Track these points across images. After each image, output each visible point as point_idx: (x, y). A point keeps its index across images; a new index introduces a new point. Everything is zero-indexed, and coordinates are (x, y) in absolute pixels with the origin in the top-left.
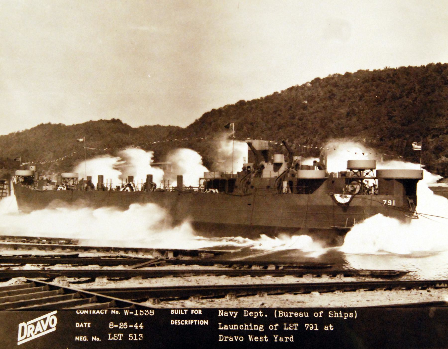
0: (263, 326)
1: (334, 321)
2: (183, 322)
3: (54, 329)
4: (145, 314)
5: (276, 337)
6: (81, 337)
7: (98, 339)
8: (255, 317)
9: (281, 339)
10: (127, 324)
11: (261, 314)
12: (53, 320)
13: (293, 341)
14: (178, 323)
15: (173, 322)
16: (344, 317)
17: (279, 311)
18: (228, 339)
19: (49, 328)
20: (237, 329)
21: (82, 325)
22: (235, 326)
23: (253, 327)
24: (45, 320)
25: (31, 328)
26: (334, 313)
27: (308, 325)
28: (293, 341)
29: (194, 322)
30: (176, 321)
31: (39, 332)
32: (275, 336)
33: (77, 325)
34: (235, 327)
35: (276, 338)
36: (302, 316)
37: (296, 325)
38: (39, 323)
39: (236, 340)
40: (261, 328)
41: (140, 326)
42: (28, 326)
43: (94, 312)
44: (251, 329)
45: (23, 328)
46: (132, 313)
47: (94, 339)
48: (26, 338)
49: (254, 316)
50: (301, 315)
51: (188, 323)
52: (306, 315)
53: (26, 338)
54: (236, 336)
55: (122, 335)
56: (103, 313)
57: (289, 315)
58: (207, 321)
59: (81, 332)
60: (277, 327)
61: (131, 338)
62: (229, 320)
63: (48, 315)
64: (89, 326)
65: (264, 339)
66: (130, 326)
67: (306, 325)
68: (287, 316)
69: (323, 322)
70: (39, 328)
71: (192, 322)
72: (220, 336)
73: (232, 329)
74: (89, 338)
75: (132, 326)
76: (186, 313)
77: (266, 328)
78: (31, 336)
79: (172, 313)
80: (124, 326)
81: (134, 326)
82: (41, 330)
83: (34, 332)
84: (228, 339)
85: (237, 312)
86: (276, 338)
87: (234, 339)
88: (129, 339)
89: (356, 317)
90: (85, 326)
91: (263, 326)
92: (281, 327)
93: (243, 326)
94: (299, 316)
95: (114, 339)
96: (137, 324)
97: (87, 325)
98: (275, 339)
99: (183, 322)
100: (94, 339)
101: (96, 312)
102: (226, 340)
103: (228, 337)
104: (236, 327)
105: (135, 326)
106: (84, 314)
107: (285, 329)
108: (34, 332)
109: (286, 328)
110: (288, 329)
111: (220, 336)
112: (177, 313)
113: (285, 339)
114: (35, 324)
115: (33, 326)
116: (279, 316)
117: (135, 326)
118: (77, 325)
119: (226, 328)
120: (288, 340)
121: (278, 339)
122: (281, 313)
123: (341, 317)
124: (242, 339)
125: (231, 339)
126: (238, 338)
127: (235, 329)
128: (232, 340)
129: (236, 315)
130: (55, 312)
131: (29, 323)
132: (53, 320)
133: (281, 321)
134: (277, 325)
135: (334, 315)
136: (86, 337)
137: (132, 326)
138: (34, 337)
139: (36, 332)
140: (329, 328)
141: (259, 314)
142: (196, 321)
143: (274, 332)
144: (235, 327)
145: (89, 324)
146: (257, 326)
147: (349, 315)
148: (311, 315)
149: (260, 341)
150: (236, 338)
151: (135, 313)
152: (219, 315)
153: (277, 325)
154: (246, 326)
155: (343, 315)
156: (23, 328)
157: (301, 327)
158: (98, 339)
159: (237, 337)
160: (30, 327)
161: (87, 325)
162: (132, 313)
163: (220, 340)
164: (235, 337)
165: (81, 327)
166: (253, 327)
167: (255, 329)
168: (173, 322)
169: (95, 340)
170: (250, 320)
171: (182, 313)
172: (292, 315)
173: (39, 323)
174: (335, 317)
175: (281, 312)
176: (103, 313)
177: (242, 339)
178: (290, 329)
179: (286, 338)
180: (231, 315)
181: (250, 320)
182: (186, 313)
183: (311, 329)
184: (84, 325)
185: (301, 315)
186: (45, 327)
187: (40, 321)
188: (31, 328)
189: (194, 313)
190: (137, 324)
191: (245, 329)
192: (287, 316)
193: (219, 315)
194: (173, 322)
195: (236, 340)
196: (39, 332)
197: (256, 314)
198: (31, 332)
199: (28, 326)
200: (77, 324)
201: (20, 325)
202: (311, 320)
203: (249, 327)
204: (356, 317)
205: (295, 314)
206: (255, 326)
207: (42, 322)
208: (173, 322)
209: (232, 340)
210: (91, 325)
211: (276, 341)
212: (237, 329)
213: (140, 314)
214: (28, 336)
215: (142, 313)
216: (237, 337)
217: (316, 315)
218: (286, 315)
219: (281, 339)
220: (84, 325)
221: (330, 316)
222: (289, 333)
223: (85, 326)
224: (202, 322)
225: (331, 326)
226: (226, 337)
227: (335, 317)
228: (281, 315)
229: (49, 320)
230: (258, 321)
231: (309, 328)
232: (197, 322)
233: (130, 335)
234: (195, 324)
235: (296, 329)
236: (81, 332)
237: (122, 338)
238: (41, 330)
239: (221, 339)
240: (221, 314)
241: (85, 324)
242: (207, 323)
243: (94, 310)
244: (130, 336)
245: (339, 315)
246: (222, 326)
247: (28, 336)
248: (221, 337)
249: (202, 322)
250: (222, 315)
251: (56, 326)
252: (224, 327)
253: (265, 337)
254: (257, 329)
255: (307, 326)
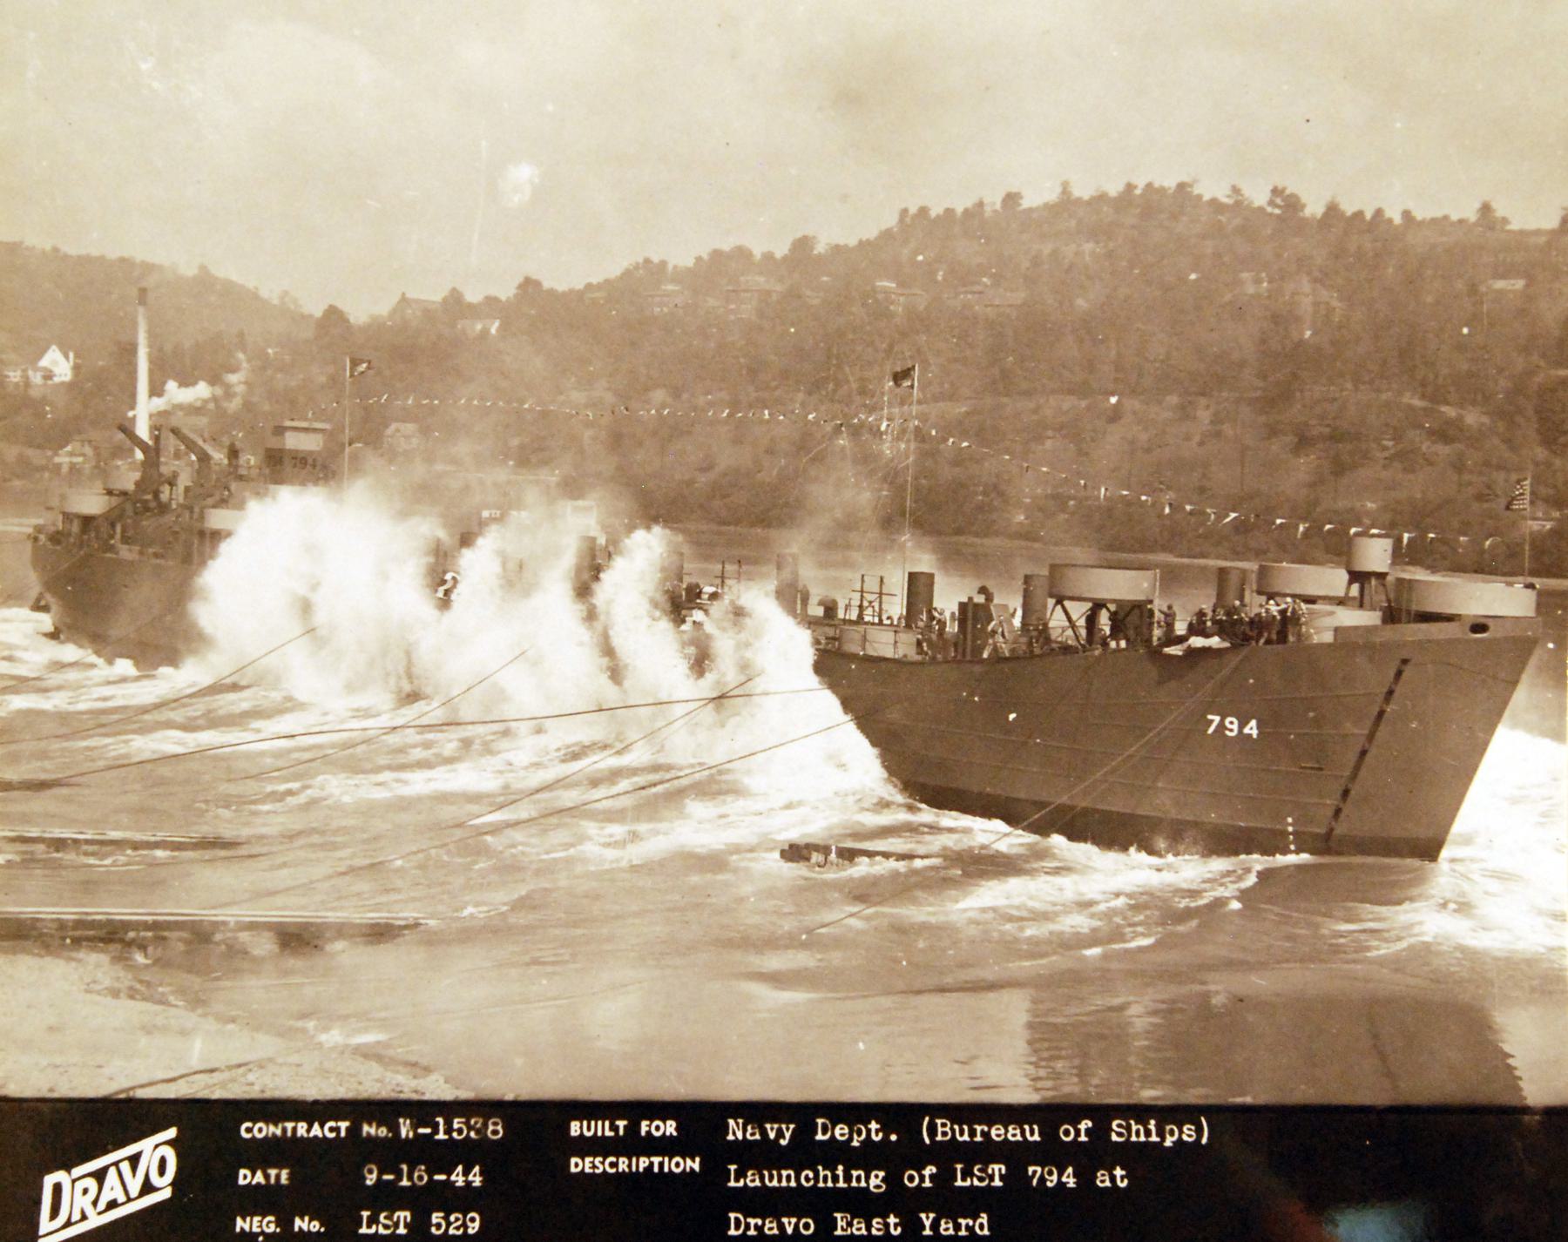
0: (882, 1174)
1: (1130, 1155)
2: (612, 1165)
3: (166, 1194)
4: (472, 1134)
5: (927, 1219)
6: (257, 1219)
7: (315, 1226)
8: (855, 1144)
9: (946, 1228)
10: (426, 1171)
11: (877, 1132)
12: (163, 1161)
13: (986, 1232)
14: (594, 1167)
15: (577, 1165)
16: (1163, 1139)
17: (939, 1122)
18: (759, 1228)
19: (148, 1188)
20: (793, 1184)
21: (259, 1178)
22: (784, 1173)
23: (848, 1178)
24: (134, 1160)
25: (85, 1191)
26: (1129, 1128)
27: (1039, 1169)
28: (986, 1232)
29: (652, 1164)
30: (588, 1160)
31: (112, 1205)
32: (923, 1216)
33: (244, 1177)
34: (783, 1179)
35: (927, 1223)
36: (1019, 1138)
37: (997, 1169)
38: (112, 1171)
39: (790, 1230)
40: (878, 1182)
41: (470, 1178)
42: (74, 1181)
43: (302, 1129)
44: (841, 1184)
45: (57, 1189)
46: (428, 1131)
47: (301, 1224)
48: (68, 1224)
49: (851, 1139)
50: (1013, 1134)
51: (630, 1166)
52: (1032, 1133)
53: (68, 1224)
54: (789, 1216)
55: (1003, 1168)
56: (333, 1135)
57: (972, 1133)
58: (698, 1159)
59: (258, 1201)
60: (931, 1176)
61: (438, 1226)
62: (763, 1155)
63: (145, 1145)
64: (284, 1180)
65: (887, 1225)
66: (437, 1177)
67: (1031, 1169)
68: (966, 1138)
69: (1097, 1153)
70: (112, 1189)
71: (644, 1162)
72: (732, 1216)
73: (775, 1183)
74: (285, 1222)
75: (443, 1177)
76: (621, 1132)
77: (893, 1180)
78: (84, 1217)
79: (573, 1133)
80: (412, 1177)
81: (449, 1174)
82: (121, 1198)
83: (95, 1203)
84: (759, 1228)
85: (792, 1126)
86: (927, 1223)
87: (781, 1227)
88: (433, 1230)
89: (1204, 1141)
90: (273, 1181)
91: (882, 1174)
92: (944, 1178)
93: (811, 1175)
94: (1006, 1139)
95: (976, 1183)
96: (460, 1168)
97: (278, 1177)
98: (924, 1228)
99: (612, 1165)
100: (301, 1224)
101: (308, 1131)
102: (752, 1232)
103: (760, 1222)
104: (858, 1179)
105: (453, 1178)
106: (266, 1138)
107: (959, 1183)
108: (95, 1203)
109: (964, 1179)
110: (968, 1183)
111: (732, 1216)
112: (591, 1134)
113: (957, 1227)
114: (100, 1175)
115: (91, 1183)
116: (939, 1138)
117: (453, 1178)
118: (244, 1177)
119: (752, 1180)
120: (969, 1229)
121: (935, 1226)
122: (945, 1129)
123: (1154, 1138)
124: (808, 1227)
125: (771, 1228)
126: (797, 1225)
127: (784, 1184)
128: (775, 1231)
129: (788, 1135)
130: (171, 1133)
131: (78, 1171)
132: (163, 1161)
133: (946, 1155)
134: (930, 1170)
135: (1130, 1135)
136: (272, 1218)
137: (443, 1177)
138: (95, 1221)
139: (102, 1205)
140: (1113, 1179)
141: (869, 1131)
142: (656, 1160)
143: (921, 1199)
144: (783, 1179)
145: (284, 1174)
146: (862, 1173)
147: (1181, 1132)
148: (1050, 1133)
149: (874, 1232)
150: (789, 1224)
151: (436, 1131)
152: (730, 1137)
153: (930, 1170)
154: (822, 1174)
155: (1161, 1134)
156: (57, 1189)
157: (1016, 1176)
158: (315, 1226)
159: (794, 1220)
160: (80, 1185)
161: (278, 1177)
162: (428, 1131)
163: (732, 1232)
164: (785, 1220)
165: (258, 1184)
166: (848, 1178)
167: (854, 1184)
168: (577, 1165)
169: (305, 1227)
170: (835, 1154)
171: (608, 1133)
172: (983, 1133)
173: (112, 1170)
174: (1134, 1138)
175: (944, 1125)
176: (333, 1135)
177: (808, 1227)
178: (382, 1231)
179: (963, 1222)
180: (772, 1135)
181: (835, 1154)
182: (621, 1132)
183: (1049, 1184)
184: (267, 1177)
185: (1013, 1134)
186: (135, 1186)
187: (116, 1164)
188: (85, 1191)
189: (649, 1133)
190: (460, 1168)
191: (821, 1185)
192: (966, 1138)
193: (730, 1137)
194: (576, 1165)
195: (790, 1230)
196: (112, 1205)
197: (859, 1134)
198: (84, 1202)
199: (74, 1181)
200: (242, 1172)
201: (49, 1181)
202: (1051, 1152)
203: (835, 1179)
204: (1204, 1141)
205: (993, 1132)
206: (855, 1173)
207: (125, 1167)
208: (576, 1165)
209: (775, 1231)
210: (291, 1177)
211: (927, 1232)
212: (793, 1184)
213: (455, 1135)
214: (74, 1219)
215: (460, 1131)
216: (794, 1220)
217: (1067, 1133)
218: (962, 1134)
219: (946, 1228)
220: (267, 1177)
221: (1114, 1138)
222: (972, 1202)
223: (273, 1181)
224: (678, 1165)
225: (1119, 1172)
226: (752, 1221)
227: (1134, 1138)
228: (944, 1134)
229: (149, 1162)
230: (868, 1157)
231: (1042, 1180)
232: (661, 1165)
233: (436, 1217)
234: (656, 1169)
235: (402, 1231)
236: (258, 1201)
237: (1002, 1177)
238: (121, 1198)
239: (737, 1228)
240: (736, 1130)
241: (273, 1172)
242: (696, 1167)
243: (477, 1115)
244: (434, 1221)
245: (1148, 1133)
246: (740, 1174)
247: (76, 1216)
248: (737, 1221)
249: (678, 1165)
250: (740, 1136)
251: (173, 1184)
252: (745, 1177)
253: (892, 1220)
254: (863, 1184)
255: (1035, 1172)
